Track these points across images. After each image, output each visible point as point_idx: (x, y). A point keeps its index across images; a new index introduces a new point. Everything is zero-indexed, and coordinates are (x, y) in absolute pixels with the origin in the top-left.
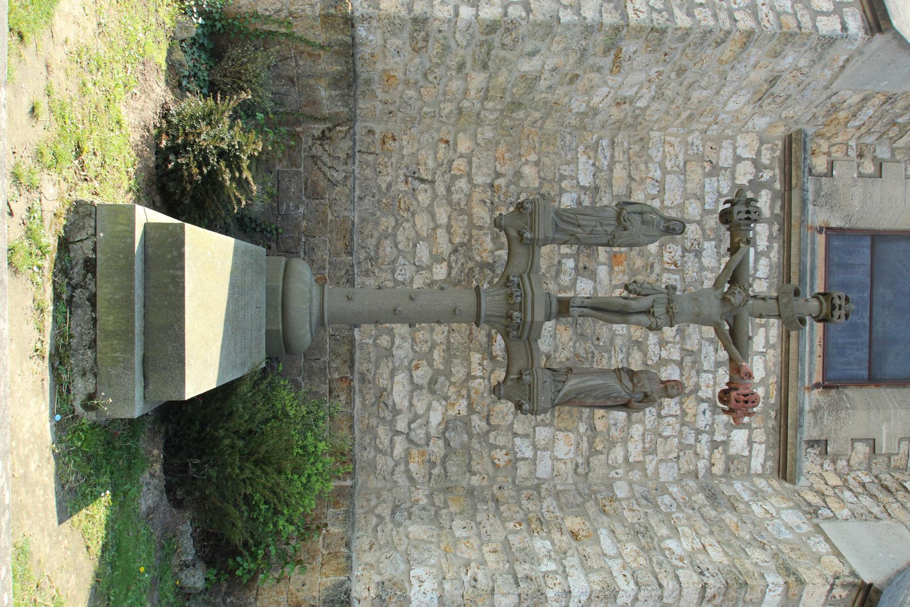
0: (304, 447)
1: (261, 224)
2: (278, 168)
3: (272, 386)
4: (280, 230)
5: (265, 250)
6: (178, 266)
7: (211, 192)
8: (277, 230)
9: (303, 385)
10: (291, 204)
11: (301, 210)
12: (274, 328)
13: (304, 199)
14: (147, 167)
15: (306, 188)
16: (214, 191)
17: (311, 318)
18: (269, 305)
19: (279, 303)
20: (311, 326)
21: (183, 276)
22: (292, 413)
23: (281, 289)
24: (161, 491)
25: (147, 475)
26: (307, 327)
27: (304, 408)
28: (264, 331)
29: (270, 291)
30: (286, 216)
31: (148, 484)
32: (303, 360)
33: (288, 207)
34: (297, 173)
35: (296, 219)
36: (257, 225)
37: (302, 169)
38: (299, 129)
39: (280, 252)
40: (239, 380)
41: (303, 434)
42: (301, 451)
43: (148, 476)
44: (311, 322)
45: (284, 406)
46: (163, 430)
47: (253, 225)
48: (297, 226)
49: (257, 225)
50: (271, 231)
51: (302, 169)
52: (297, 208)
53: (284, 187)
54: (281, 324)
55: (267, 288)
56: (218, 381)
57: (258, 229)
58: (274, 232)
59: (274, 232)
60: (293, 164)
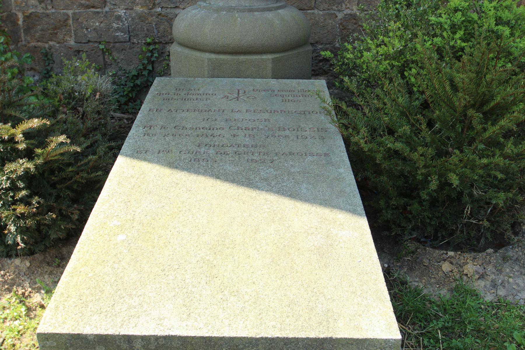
0: (454, 28)
1: (143, 64)
2: (72, 43)
3: (352, 69)
4: (149, 40)
5: (157, 80)
6: (125, 346)
7: (63, 175)
8: (149, 44)
9: (348, 11)
10: (115, 25)
11: (121, 12)
12: (270, 66)
13: (107, 9)
14: (30, 273)
15: (93, 7)
16: (60, 170)
17: (258, 10)
18: (238, 73)
19: (233, 58)
20: (269, 10)
21: (145, 339)
22: (398, 45)
23: (213, 56)
24: (505, 259)
25: (480, 285)
26: (269, 15)
27: (393, 25)
28: (273, 82)
29: (217, 71)
30: (130, 32)
31: (494, 285)
32: (316, 11)
33: (118, 29)
34: (76, 18)
35: (133, 19)
36: (145, 68)
37: (70, 12)
38: (20, 16)
39: (164, 55)
40: (347, 142)
41: (432, 31)
42: (460, 34)
43: (482, 283)
44: (263, 10)
45: (387, 57)
46: (412, 246)
47: (145, 73)
48: (142, 17)
49: (145, 68)
50: (151, 52)
51: (70, 12)
52: (119, 18)
53: (94, 34)
54: (265, 57)
55: (213, 76)
56: (354, 212)
57: (150, 67)
58: (151, 47)
59: (151, 47)
60: (65, 23)
